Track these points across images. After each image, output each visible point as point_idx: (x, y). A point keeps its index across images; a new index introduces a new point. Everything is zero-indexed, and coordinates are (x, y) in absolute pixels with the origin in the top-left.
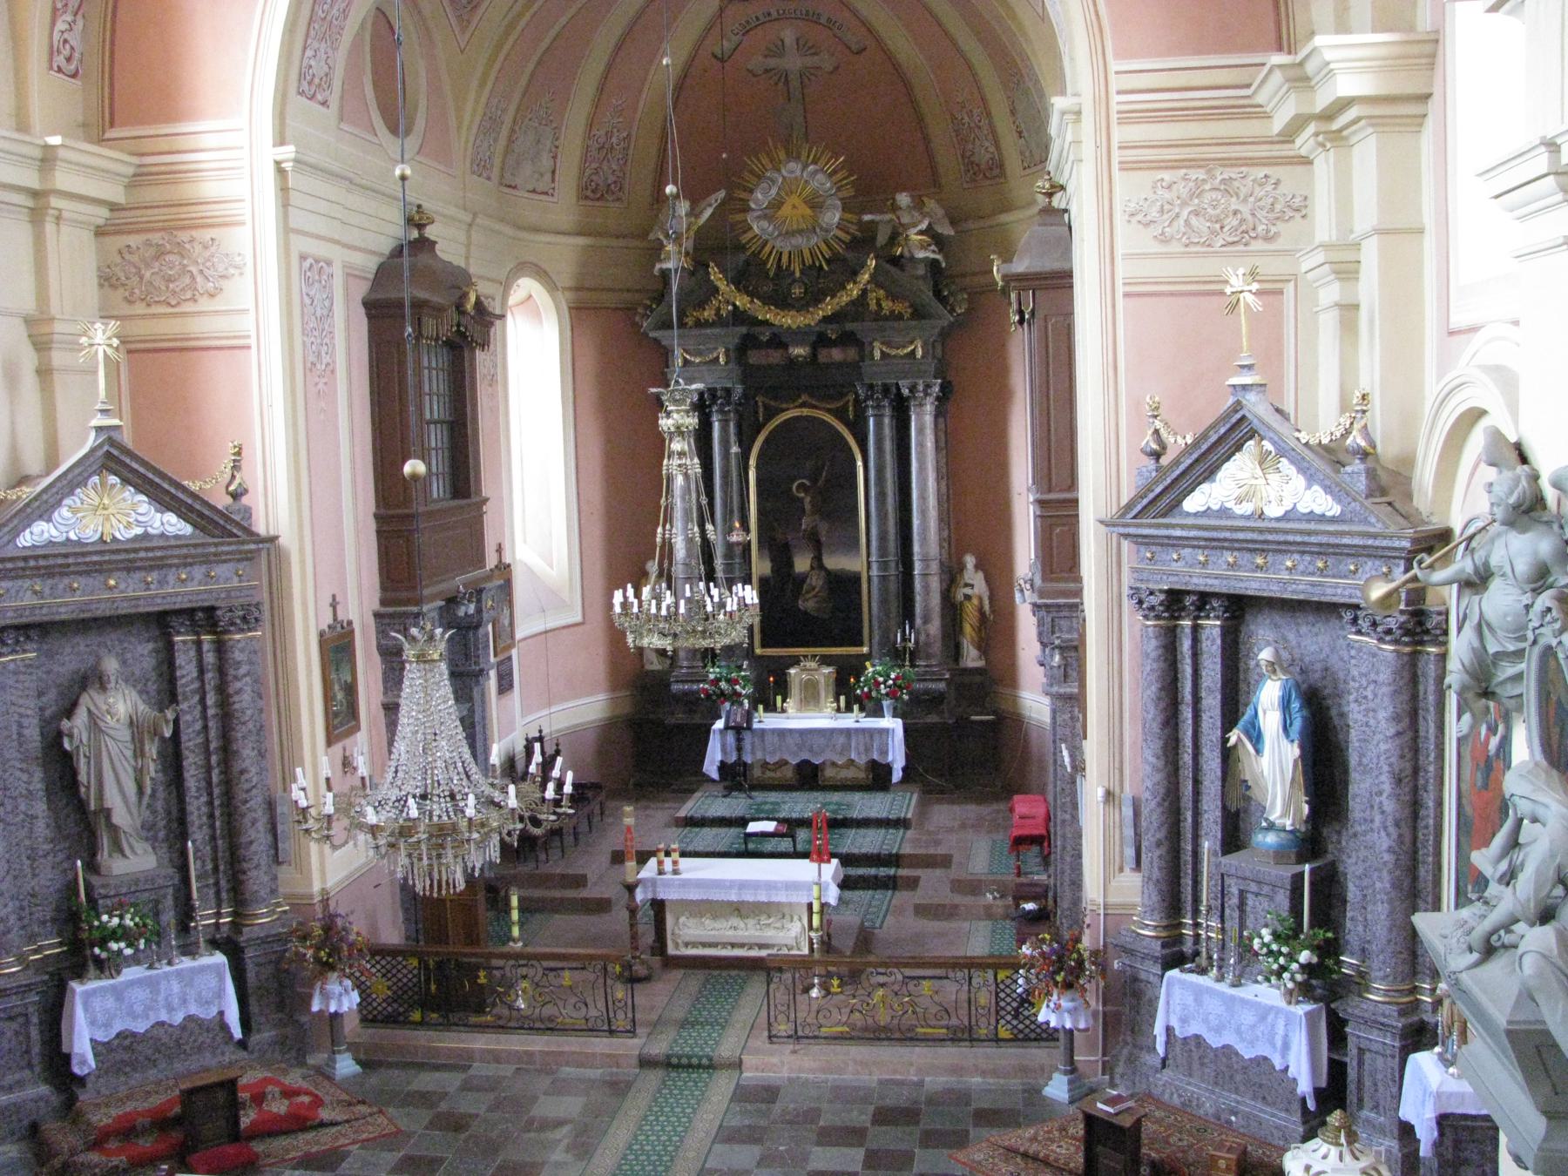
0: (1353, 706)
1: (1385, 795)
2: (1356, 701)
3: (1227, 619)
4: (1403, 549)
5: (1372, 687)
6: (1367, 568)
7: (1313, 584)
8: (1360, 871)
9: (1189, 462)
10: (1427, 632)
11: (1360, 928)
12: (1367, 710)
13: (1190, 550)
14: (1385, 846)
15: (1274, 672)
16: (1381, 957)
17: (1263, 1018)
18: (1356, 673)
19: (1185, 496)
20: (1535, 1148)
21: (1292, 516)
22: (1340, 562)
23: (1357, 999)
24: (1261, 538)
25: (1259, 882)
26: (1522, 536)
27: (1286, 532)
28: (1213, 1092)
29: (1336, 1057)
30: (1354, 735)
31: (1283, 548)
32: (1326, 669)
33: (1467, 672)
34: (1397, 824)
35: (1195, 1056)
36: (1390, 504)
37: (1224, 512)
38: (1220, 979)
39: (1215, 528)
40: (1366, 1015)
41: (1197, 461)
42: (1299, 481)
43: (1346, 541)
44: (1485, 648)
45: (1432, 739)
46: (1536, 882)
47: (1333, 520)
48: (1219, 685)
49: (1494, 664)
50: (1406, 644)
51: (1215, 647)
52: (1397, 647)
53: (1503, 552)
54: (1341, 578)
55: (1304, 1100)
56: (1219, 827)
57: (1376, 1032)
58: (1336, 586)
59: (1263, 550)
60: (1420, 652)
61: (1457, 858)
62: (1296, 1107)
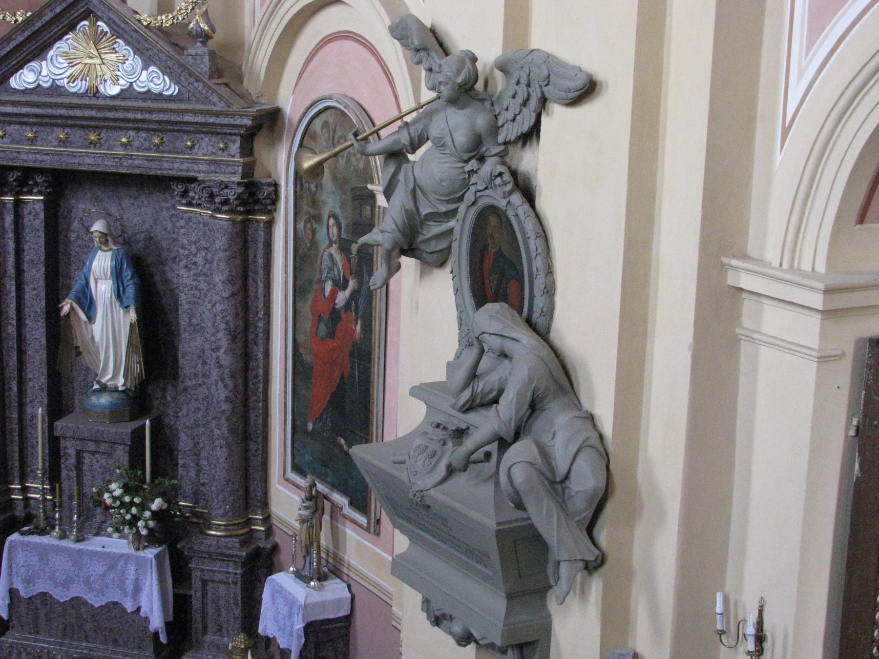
0: (182, 272)
1: (222, 351)
2: (186, 267)
3: (49, 194)
4: (245, 126)
5: (203, 253)
6: (203, 144)
7: (150, 159)
8: (191, 421)
9: (21, 38)
10: (257, 202)
11: (192, 473)
12: (198, 275)
13: (18, 127)
14: (223, 396)
15: (106, 243)
16: (221, 496)
17: (112, 567)
18: (185, 242)
19: (12, 74)
20: (501, 625)
21: (128, 95)
22: (177, 139)
23: (200, 537)
24: (99, 115)
25: (96, 441)
26: (464, 111)
27: (127, 109)
28: (62, 644)
29: (181, 592)
30: (183, 298)
31: (119, 125)
32: (151, 239)
33: (400, 231)
34: (232, 377)
35: (42, 613)
36: (226, 85)
37: (56, 89)
38: (63, 536)
39: (51, 106)
40: (212, 549)
41: (29, 38)
42: (134, 62)
43: (187, 118)
44: (417, 209)
45: (262, 298)
46: (517, 403)
47: (170, 99)
48: (43, 258)
49: (422, 223)
50: (241, 213)
51: (38, 221)
52: (233, 216)
53: (443, 125)
54: (178, 153)
55: (156, 635)
56: (45, 393)
57: (219, 564)
58: (174, 160)
59: (97, 127)
60: (249, 220)
61: (293, 401)
62: (149, 643)
